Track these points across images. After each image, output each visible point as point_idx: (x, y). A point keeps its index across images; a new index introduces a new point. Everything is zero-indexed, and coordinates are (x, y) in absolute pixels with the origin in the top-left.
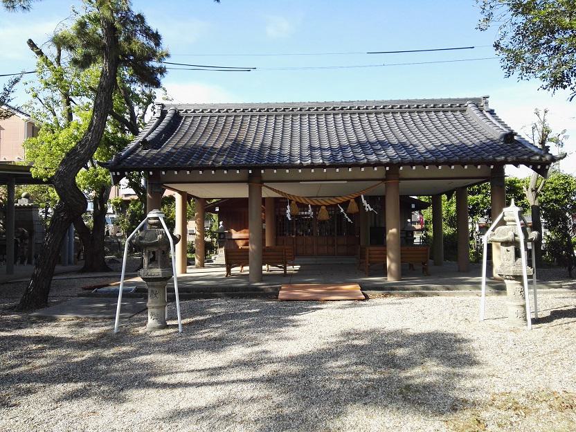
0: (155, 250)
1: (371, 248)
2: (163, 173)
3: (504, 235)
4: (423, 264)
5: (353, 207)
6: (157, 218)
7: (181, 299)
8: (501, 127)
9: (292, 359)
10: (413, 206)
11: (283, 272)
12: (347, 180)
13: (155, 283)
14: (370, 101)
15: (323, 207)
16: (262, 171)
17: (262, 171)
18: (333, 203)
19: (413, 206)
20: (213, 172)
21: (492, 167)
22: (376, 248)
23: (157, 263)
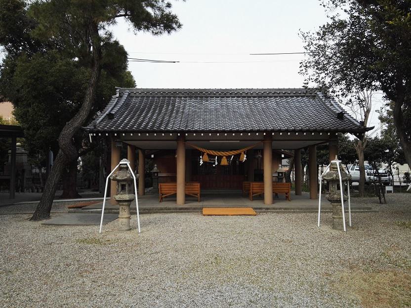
0: (124, 183)
1: (254, 183)
2: (124, 135)
3: (331, 177)
4: (287, 194)
5: (274, 178)
6: (126, 164)
7: (140, 214)
8: (337, 107)
9: (247, 207)
10: (283, 156)
11: (277, 175)
12: (240, 140)
13: (124, 203)
14: (255, 89)
15: (224, 157)
16: (187, 135)
17: (187, 135)
18: (226, 152)
19: (283, 156)
20: (147, 134)
21: (329, 134)
22: (257, 183)
23: (125, 191)
